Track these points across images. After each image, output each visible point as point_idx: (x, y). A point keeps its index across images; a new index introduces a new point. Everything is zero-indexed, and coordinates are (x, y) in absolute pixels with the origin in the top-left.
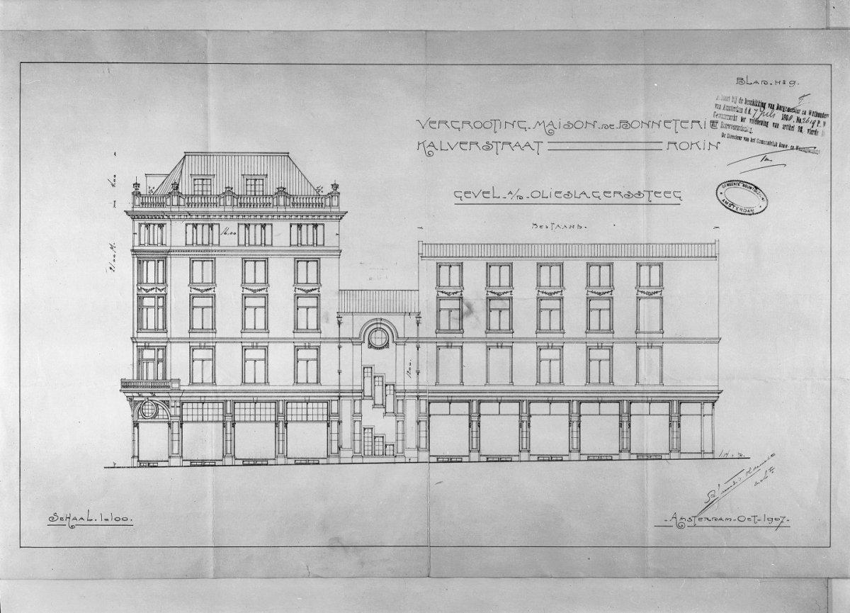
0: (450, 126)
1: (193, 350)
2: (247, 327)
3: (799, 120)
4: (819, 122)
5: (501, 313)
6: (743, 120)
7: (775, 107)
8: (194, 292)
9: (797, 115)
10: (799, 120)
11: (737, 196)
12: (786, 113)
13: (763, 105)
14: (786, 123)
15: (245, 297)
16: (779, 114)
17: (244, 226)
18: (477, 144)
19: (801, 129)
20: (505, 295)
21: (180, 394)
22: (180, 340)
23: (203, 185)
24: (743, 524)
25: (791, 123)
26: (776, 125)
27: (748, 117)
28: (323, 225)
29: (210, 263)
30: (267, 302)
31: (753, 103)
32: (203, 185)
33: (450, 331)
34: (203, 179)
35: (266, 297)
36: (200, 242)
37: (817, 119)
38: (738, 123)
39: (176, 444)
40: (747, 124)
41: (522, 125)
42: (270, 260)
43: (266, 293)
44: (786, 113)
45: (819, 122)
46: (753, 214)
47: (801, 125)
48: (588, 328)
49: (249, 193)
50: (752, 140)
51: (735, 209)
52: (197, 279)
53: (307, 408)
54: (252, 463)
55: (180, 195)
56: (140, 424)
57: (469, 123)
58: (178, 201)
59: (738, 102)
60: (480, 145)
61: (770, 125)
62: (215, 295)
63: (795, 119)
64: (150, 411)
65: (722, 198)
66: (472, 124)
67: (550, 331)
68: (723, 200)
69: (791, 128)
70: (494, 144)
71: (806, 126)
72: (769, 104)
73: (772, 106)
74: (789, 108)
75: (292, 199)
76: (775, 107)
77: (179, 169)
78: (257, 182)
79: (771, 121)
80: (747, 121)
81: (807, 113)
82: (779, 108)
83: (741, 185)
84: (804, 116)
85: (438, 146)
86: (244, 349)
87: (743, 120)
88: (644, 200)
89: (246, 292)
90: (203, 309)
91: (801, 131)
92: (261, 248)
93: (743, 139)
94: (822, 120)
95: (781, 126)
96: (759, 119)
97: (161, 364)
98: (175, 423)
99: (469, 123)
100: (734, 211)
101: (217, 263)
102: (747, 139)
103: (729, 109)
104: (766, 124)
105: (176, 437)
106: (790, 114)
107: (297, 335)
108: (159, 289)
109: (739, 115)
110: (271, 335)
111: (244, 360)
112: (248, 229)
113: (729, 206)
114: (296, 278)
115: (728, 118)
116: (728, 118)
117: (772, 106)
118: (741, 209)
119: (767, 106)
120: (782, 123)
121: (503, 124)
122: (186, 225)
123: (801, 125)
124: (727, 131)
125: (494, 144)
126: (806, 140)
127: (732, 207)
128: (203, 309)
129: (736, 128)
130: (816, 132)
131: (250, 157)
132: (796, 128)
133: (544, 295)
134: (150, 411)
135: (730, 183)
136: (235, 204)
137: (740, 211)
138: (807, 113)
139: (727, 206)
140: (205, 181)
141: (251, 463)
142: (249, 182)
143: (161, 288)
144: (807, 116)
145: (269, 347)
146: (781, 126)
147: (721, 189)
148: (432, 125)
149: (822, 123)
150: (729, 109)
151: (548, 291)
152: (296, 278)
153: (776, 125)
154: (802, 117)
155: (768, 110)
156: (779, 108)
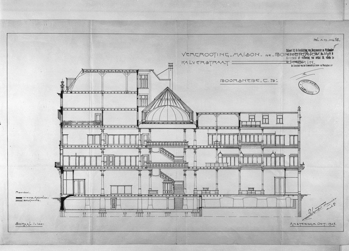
0: (204, 55)
3: (322, 54)
4: (330, 53)
5: (234, 137)
6: (299, 58)
7: (311, 51)
9: (321, 52)
10: (322, 54)
11: (308, 87)
12: (316, 52)
13: (306, 50)
14: (317, 56)
18: (203, 62)
19: (323, 58)
24: (319, 225)
25: (319, 56)
27: (301, 56)
31: (302, 50)
38: (297, 60)
41: (227, 55)
46: (313, 94)
47: (323, 56)
50: (304, 66)
51: (305, 92)
57: (203, 54)
59: (296, 51)
60: (205, 63)
63: (320, 54)
65: (301, 86)
66: (204, 54)
68: (301, 88)
69: (319, 58)
70: (210, 62)
71: (325, 56)
73: (310, 50)
76: (311, 51)
80: (301, 58)
81: (325, 50)
82: (313, 50)
83: (309, 82)
87: (299, 58)
88: (333, 225)
91: (323, 58)
94: (331, 52)
95: (315, 58)
96: (306, 57)
99: (203, 54)
100: (305, 92)
102: (302, 66)
104: (309, 58)
106: (318, 52)
113: (303, 90)
115: (293, 58)
116: (293, 58)
118: (308, 92)
119: (308, 51)
121: (219, 54)
123: (323, 56)
125: (210, 62)
126: (326, 61)
127: (304, 91)
129: (296, 62)
130: (330, 58)
132: (321, 58)
135: (304, 81)
138: (325, 50)
139: (303, 90)
144: (325, 52)
146: (315, 58)
147: (301, 83)
148: (188, 55)
149: (331, 54)
153: (313, 58)
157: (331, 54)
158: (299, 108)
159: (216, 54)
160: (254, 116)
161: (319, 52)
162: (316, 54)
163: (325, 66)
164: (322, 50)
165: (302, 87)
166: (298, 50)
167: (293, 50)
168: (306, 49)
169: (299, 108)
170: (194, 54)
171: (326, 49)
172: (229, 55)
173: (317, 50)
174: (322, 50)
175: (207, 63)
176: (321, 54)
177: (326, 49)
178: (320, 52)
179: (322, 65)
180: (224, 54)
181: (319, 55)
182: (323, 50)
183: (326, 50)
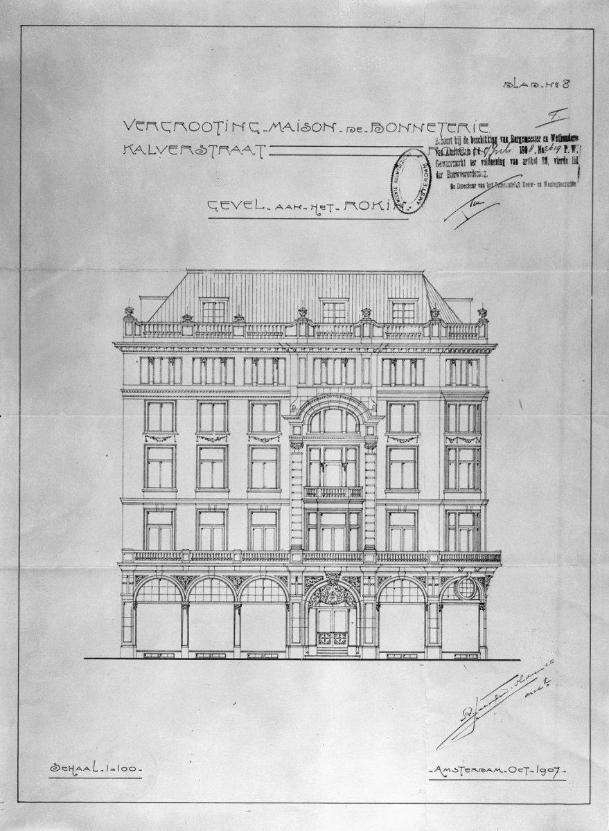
0: (358, 207)
1: (148, 513)
2: (391, 487)
3: (541, 150)
6: (473, 163)
7: (510, 140)
8: (150, 441)
10: (541, 150)
12: (524, 144)
13: (494, 141)
15: (200, 448)
16: (516, 147)
17: (147, 360)
20: (271, 442)
21: (439, 570)
22: (431, 502)
23: (334, 310)
26: (515, 162)
27: (479, 158)
28: (181, 358)
29: (413, 406)
30: (174, 455)
32: (214, 310)
33: (212, 489)
34: (405, 304)
35: (416, 449)
36: (209, 381)
37: (563, 144)
38: (468, 168)
39: (433, 632)
40: (479, 167)
41: (254, 127)
42: (231, 403)
43: (225, 443)
44: (524, 144)
45: (566, 147)
48: (447, 488)
49: (206, 320)
52: (206, 426)
53: (159, 587)
54: (259, 656)
55: (373, 324)
56: (192, 606)
58: (439, 331)
61: (508, 162)
62: (279, 446)
63: (536, 149)
64: (465, 586)
66: (357, 205)
67: (212, 489)
68: (418, 203)
72: (501, 138)
73: (505, 140)
74: (526, 138)
75: (143, 327)
76: (510, 140)
77: (429, 288)
78: (217, 306)
79: (507, 158)
80: (479, 163)
81: (550, 139)
82: (514, 140)
84: (546, 144)
85: (145, 150)
86: (147, 512)
87: (473, 163)
89: (253, 442)
90: (403, 464)
91: (546, 163)
92: (168, 388)
93: (477, 186)
94: (569, 144)
95: (521, 161)
97: (354, 533)
98: (295, 605)
101: (421, 407)
103: (452, 153)
104: (502, 162)
105: (433, 623)
106: (529, 145)
107: (199, 495)
108: (450, 439)
109: (468, 159)
110: (422, 496)
111: (147, 526)
112: (415, 364)
114: (199, 423)
115: (455, 164)
117: (505, 140)
118: (426, 180)
119: (499, 140)
120: (521, 157)
121: (230, 126)
122: (194, 359)
123: (544, 155)
124: (456, 181)
128: (403, 464)
129: (464, 174)
130: (564, 160)
131: (314, 276)
132: (540, 161)
133: (154, 442)
134: (465, 586)
136: (138, 333)
137: (428, 180)
140: (407, 306)
141: (205, 656)
142: (206, 306)
143: (452, 437)
145: (281, 511)
150: (452, 153)
151: (261, 437)
152: (199, 423)
153: (515, 162)
154: (543, 144)
155: (501, 146)
156: (514, 140)
157: (570, 149)
158: (483, 312)
159: (222, 126)
160: (232, 382)
161: (532, 143)
162: (524, 150)
163: (550, 185)
164: (542, 139)
165: (415, 202)
166: (470, 140)
167: (453, 141)
168: (494, 136)
169: (483, 312)
170: (159, 125)
171: (553, 136)
172: (260, 127)
173: (526, 140)
174: (542, 139)
175: (202, 151)
176: (539, 149)
177: (553, 136)
178: (536, 145)
179: (543, 185)
180: (246, 126)
181: (532, 152)
182: (546, 139)
183: (553, 139)
